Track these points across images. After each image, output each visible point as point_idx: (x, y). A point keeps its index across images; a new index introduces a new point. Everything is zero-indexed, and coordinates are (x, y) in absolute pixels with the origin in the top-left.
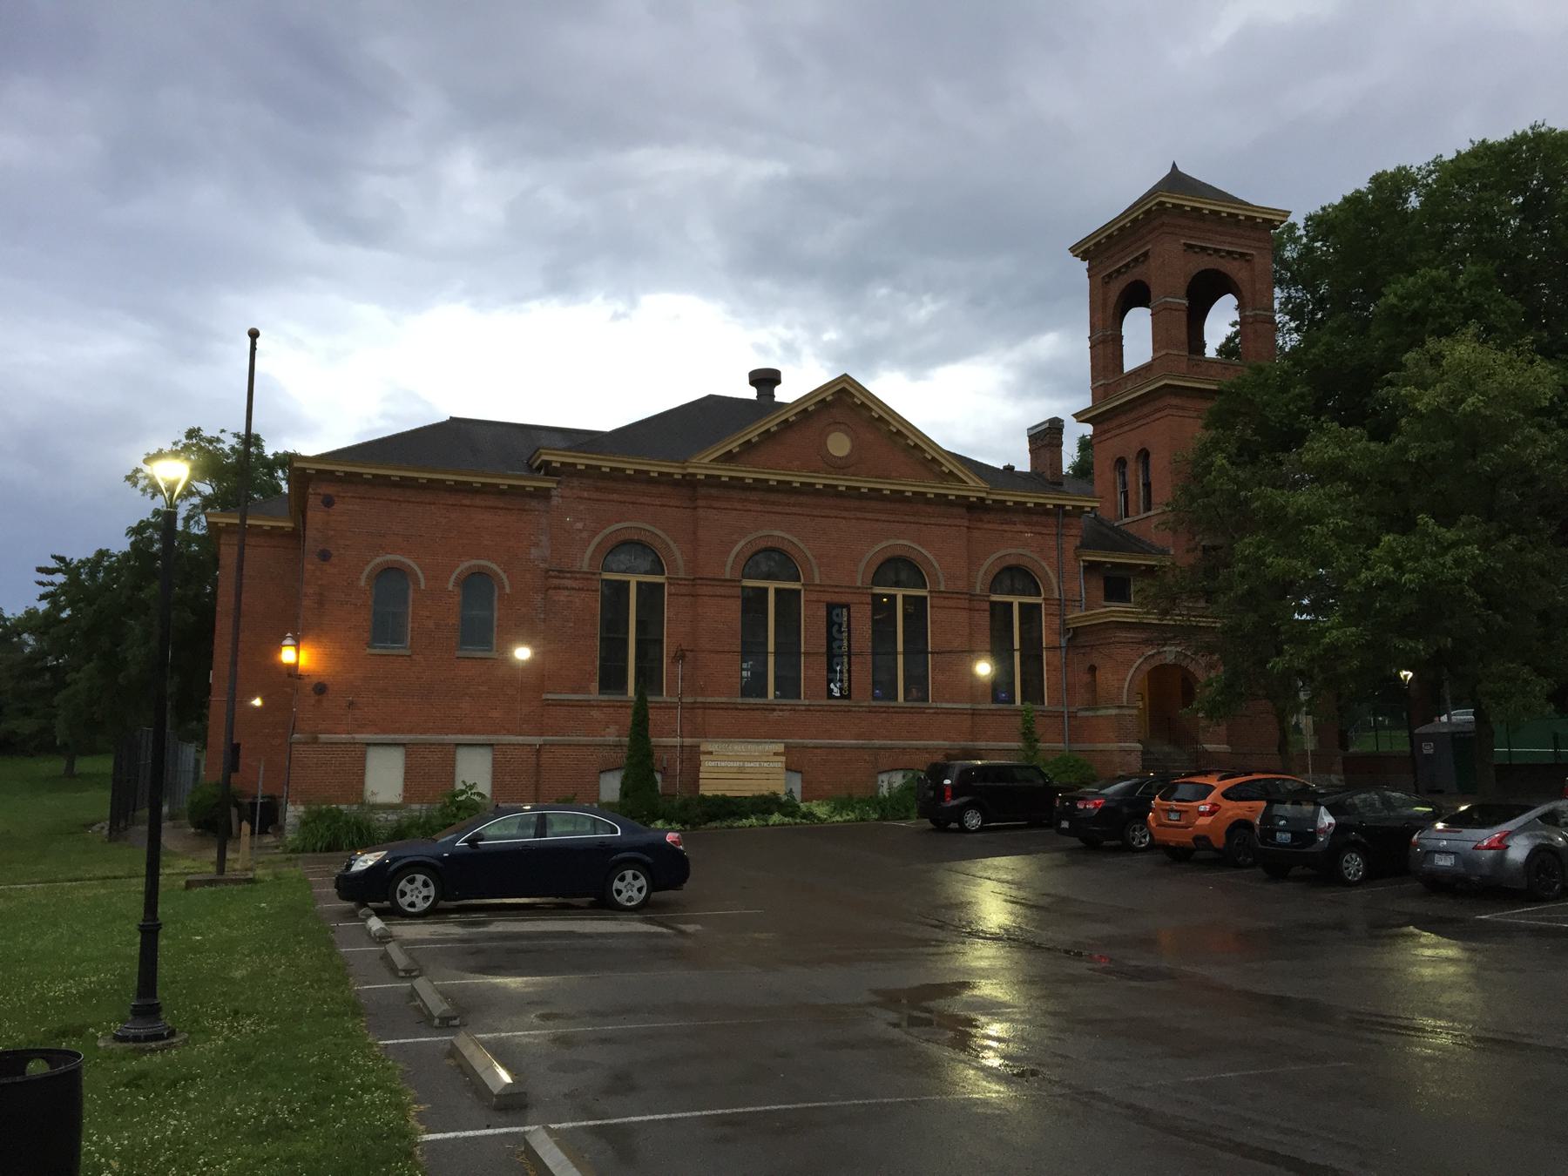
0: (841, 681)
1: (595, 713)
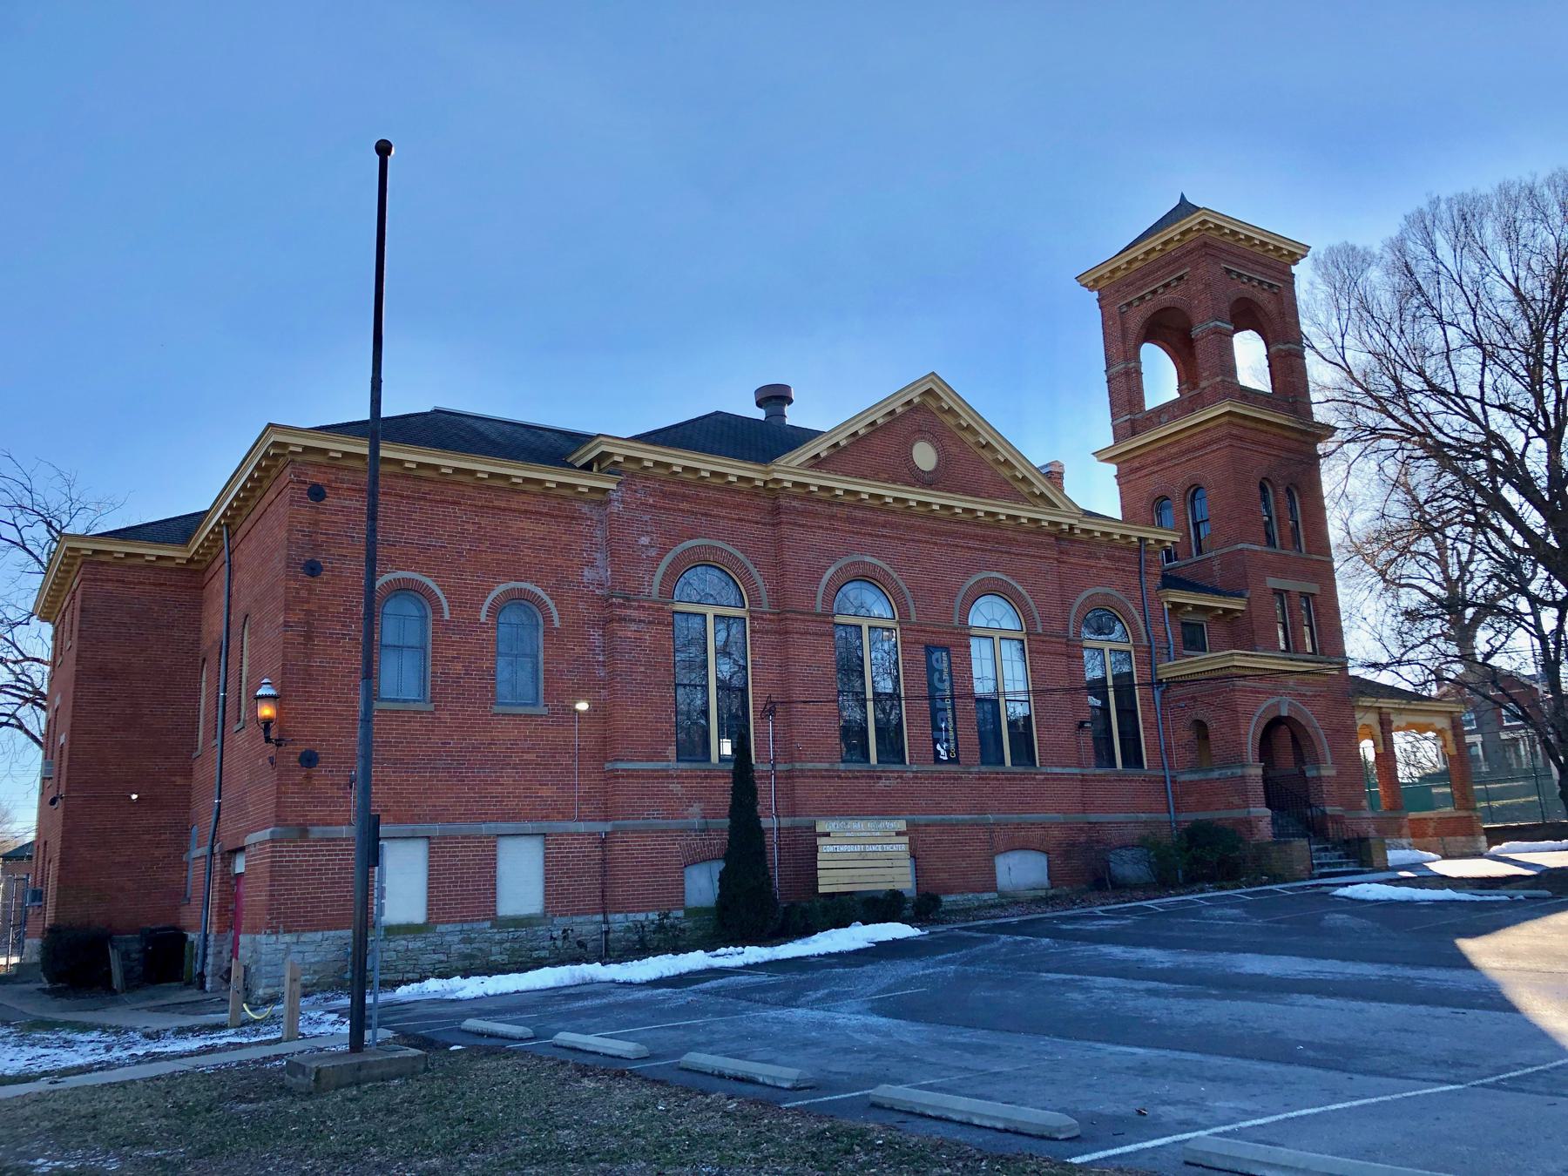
1: (675, 787)
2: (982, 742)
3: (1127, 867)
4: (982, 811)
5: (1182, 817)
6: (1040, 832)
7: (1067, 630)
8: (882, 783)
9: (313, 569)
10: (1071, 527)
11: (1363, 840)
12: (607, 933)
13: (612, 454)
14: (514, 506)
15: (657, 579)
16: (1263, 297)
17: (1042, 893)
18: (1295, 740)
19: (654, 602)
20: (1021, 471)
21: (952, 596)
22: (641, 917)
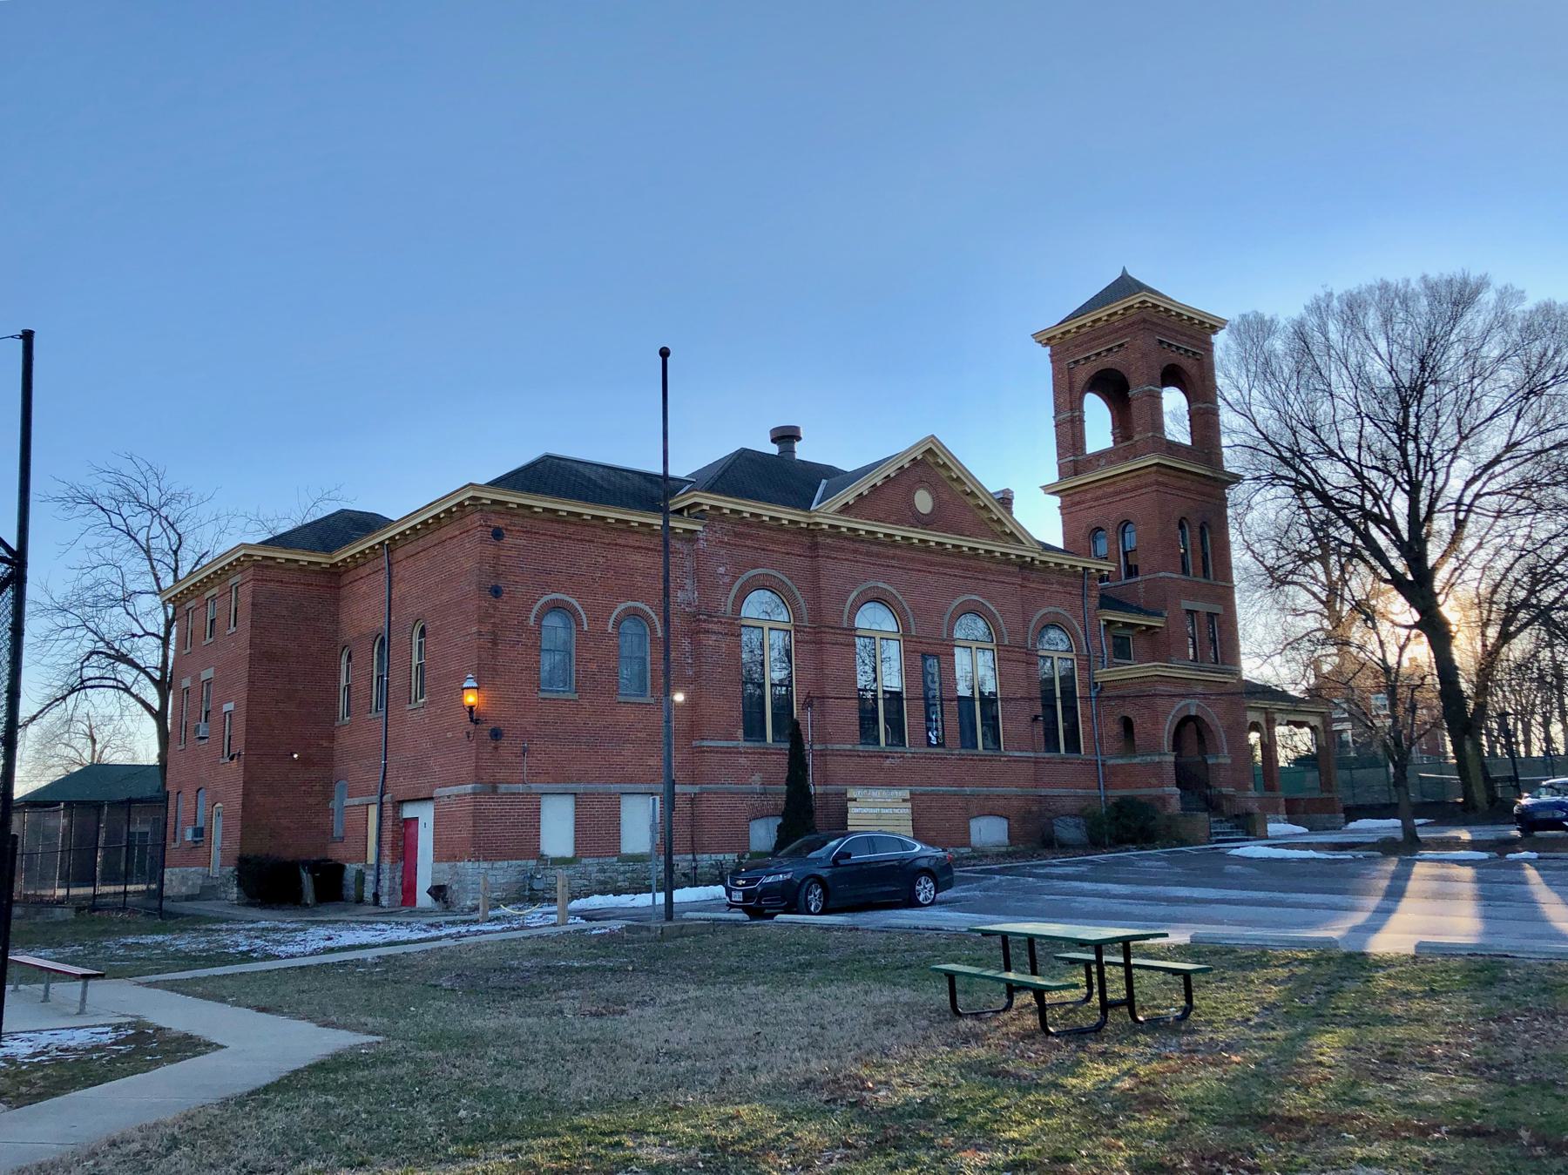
1: (742, 760)
2: (962, 733)
3: (1068, 831)
5: (1109, 793)
6: (1002, 802)
9: (496, 592)
11: (1249, 814)
14: (631, 542)
16: (1187, 364)
18: (1199, 733)
20: (984, 500)
22: (720, 857)
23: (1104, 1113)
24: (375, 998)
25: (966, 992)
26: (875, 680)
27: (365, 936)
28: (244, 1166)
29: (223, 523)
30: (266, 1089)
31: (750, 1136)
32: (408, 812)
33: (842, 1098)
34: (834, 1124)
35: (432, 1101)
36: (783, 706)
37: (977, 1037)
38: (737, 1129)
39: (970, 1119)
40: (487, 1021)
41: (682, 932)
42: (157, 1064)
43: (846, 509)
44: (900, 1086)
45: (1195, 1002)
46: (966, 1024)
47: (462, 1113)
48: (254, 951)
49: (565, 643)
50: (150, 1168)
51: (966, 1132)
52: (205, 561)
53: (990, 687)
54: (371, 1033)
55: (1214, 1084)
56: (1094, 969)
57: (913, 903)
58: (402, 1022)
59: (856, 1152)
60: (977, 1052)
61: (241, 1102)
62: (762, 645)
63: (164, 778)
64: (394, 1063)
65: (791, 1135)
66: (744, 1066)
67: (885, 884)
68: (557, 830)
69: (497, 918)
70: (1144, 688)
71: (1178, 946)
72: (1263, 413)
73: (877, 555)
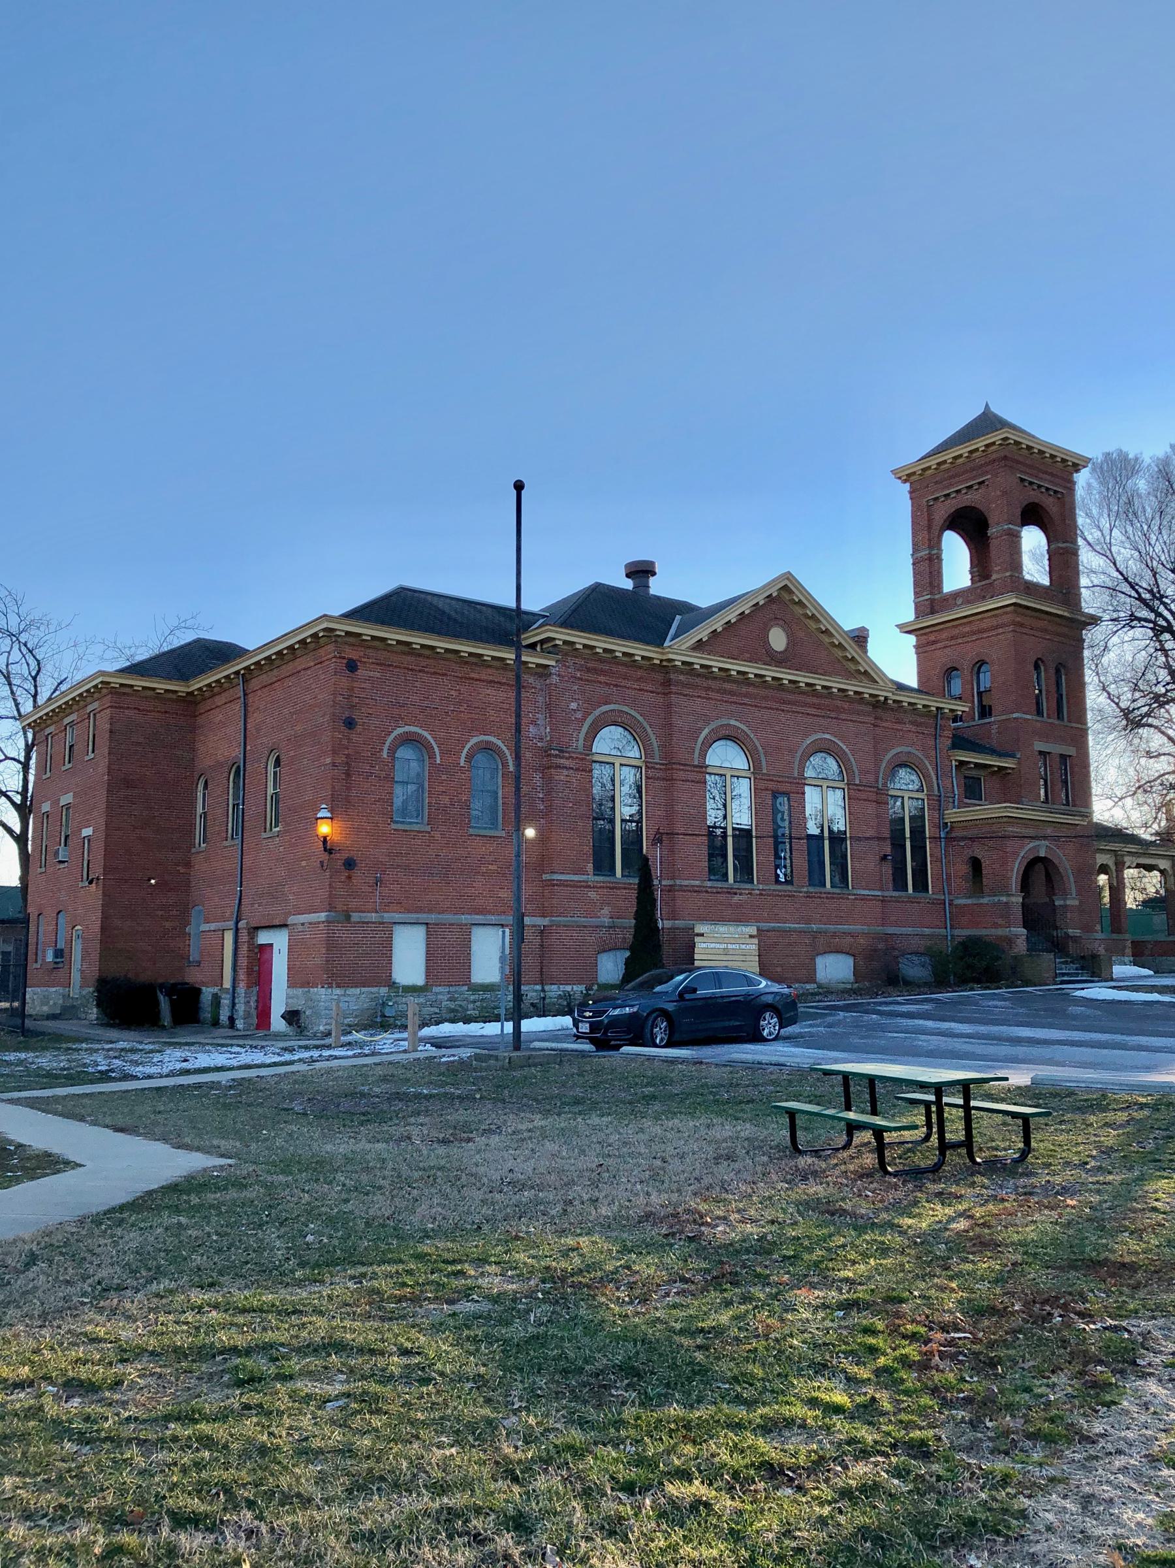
0: (785, 867)
1: (592, 895)
3: (914, 969)
4: (808, 921)
5: (957, 932)
6: (849, 939)
7: (877, 781)
8: (736, 898)
9: (350, 723)
10: (886, 698)
11: (1094, 957)
12: (544, 998)
13: (554, 639)
14: (484, 677)
15: (582, 735)
16: (1049, 502)
17: (849, 986)
18: (1049, 878)
19: (581, 753)
21: (793, 751)
22: (568, 988)
23: (936, 1254)
24: (229, 1121)
25: (806, 1129)
26: (725, 817)
27: (219, 1059)
28: (99, 1283)
29: (81, 650)
30: (122, 1208)
31: (589, 1268)
32: (263, 938)
33: (681, 1232)
34: (671, 1258)
35: (281, 1224)
36: (633, 841)
37: (815, 1174)
38: (577, 1261)
39: (806, 1257)
40: (339, 1146)
41: (529, 1062)
42: (18, 1180)
43: (699, 646)
44: (735, 1226)
45: (1033, 1144)
46: (804, 1161)
47: (310, 1238)
48: (112, 1071)
49: (418, 774)
50: (9, 1283)
51: (800, 1270)
52: (63, 687)
53: (840, 825)
54: (222, 1156)
55: (1049, 1227)
56: (934, 1109)
57: (756, 1037)
58: (253, 1146)
59: (693, 1287)
60: (815, 1189)
61: (97, 1220)
62: (613, 780)
63: (25, 900)
64: (245, 1186)
65: (629, 1268)
66: (586, 1197)
67: (730, 1018)
68: (409, 959)
69: (349, 1044)
70: (994, 828)
71: (1019, 1088)
72: (1124, 554)
73: (732, 693)
